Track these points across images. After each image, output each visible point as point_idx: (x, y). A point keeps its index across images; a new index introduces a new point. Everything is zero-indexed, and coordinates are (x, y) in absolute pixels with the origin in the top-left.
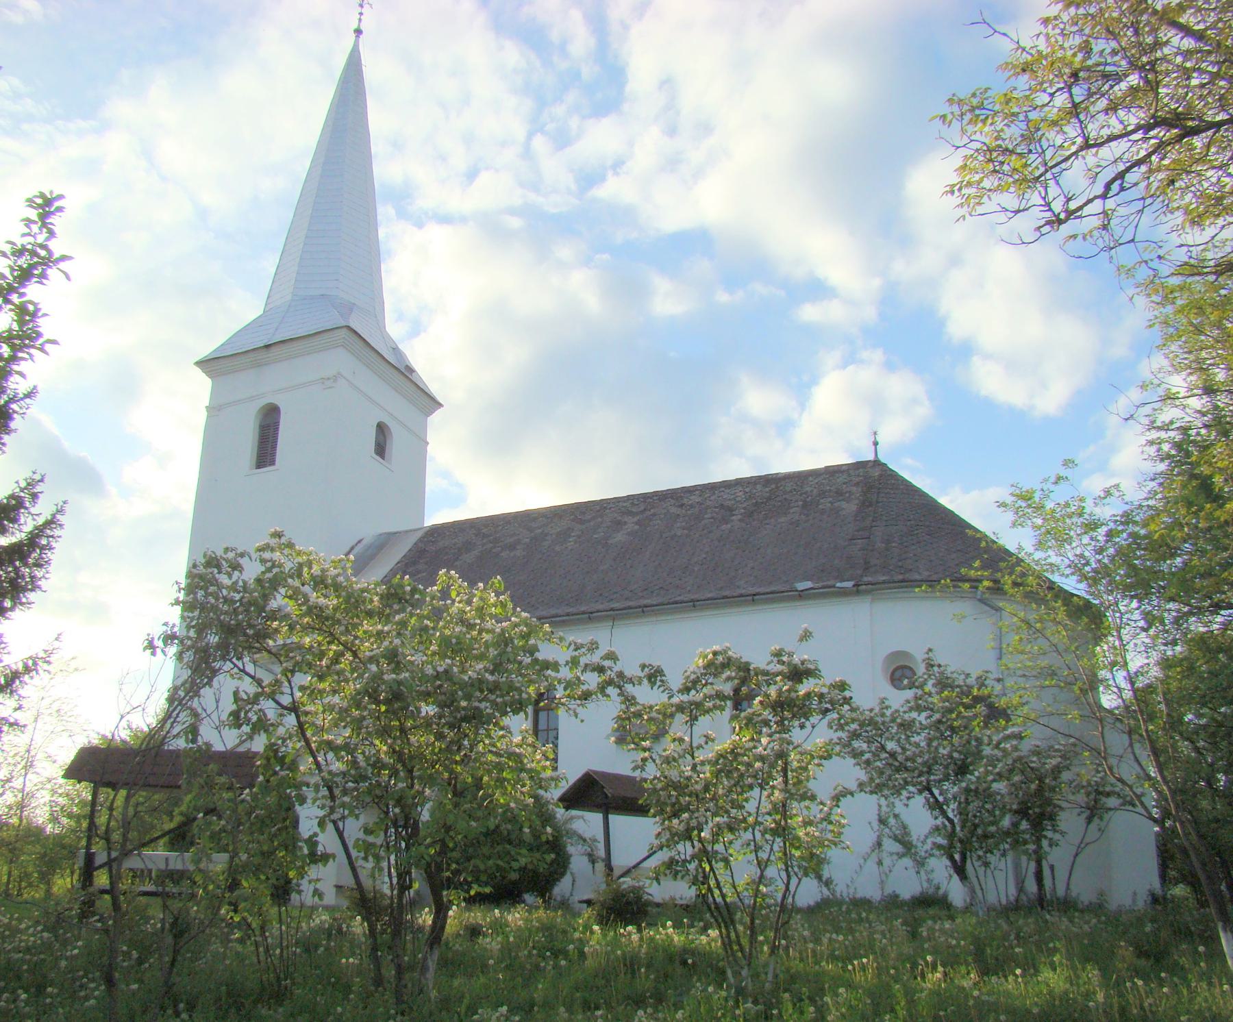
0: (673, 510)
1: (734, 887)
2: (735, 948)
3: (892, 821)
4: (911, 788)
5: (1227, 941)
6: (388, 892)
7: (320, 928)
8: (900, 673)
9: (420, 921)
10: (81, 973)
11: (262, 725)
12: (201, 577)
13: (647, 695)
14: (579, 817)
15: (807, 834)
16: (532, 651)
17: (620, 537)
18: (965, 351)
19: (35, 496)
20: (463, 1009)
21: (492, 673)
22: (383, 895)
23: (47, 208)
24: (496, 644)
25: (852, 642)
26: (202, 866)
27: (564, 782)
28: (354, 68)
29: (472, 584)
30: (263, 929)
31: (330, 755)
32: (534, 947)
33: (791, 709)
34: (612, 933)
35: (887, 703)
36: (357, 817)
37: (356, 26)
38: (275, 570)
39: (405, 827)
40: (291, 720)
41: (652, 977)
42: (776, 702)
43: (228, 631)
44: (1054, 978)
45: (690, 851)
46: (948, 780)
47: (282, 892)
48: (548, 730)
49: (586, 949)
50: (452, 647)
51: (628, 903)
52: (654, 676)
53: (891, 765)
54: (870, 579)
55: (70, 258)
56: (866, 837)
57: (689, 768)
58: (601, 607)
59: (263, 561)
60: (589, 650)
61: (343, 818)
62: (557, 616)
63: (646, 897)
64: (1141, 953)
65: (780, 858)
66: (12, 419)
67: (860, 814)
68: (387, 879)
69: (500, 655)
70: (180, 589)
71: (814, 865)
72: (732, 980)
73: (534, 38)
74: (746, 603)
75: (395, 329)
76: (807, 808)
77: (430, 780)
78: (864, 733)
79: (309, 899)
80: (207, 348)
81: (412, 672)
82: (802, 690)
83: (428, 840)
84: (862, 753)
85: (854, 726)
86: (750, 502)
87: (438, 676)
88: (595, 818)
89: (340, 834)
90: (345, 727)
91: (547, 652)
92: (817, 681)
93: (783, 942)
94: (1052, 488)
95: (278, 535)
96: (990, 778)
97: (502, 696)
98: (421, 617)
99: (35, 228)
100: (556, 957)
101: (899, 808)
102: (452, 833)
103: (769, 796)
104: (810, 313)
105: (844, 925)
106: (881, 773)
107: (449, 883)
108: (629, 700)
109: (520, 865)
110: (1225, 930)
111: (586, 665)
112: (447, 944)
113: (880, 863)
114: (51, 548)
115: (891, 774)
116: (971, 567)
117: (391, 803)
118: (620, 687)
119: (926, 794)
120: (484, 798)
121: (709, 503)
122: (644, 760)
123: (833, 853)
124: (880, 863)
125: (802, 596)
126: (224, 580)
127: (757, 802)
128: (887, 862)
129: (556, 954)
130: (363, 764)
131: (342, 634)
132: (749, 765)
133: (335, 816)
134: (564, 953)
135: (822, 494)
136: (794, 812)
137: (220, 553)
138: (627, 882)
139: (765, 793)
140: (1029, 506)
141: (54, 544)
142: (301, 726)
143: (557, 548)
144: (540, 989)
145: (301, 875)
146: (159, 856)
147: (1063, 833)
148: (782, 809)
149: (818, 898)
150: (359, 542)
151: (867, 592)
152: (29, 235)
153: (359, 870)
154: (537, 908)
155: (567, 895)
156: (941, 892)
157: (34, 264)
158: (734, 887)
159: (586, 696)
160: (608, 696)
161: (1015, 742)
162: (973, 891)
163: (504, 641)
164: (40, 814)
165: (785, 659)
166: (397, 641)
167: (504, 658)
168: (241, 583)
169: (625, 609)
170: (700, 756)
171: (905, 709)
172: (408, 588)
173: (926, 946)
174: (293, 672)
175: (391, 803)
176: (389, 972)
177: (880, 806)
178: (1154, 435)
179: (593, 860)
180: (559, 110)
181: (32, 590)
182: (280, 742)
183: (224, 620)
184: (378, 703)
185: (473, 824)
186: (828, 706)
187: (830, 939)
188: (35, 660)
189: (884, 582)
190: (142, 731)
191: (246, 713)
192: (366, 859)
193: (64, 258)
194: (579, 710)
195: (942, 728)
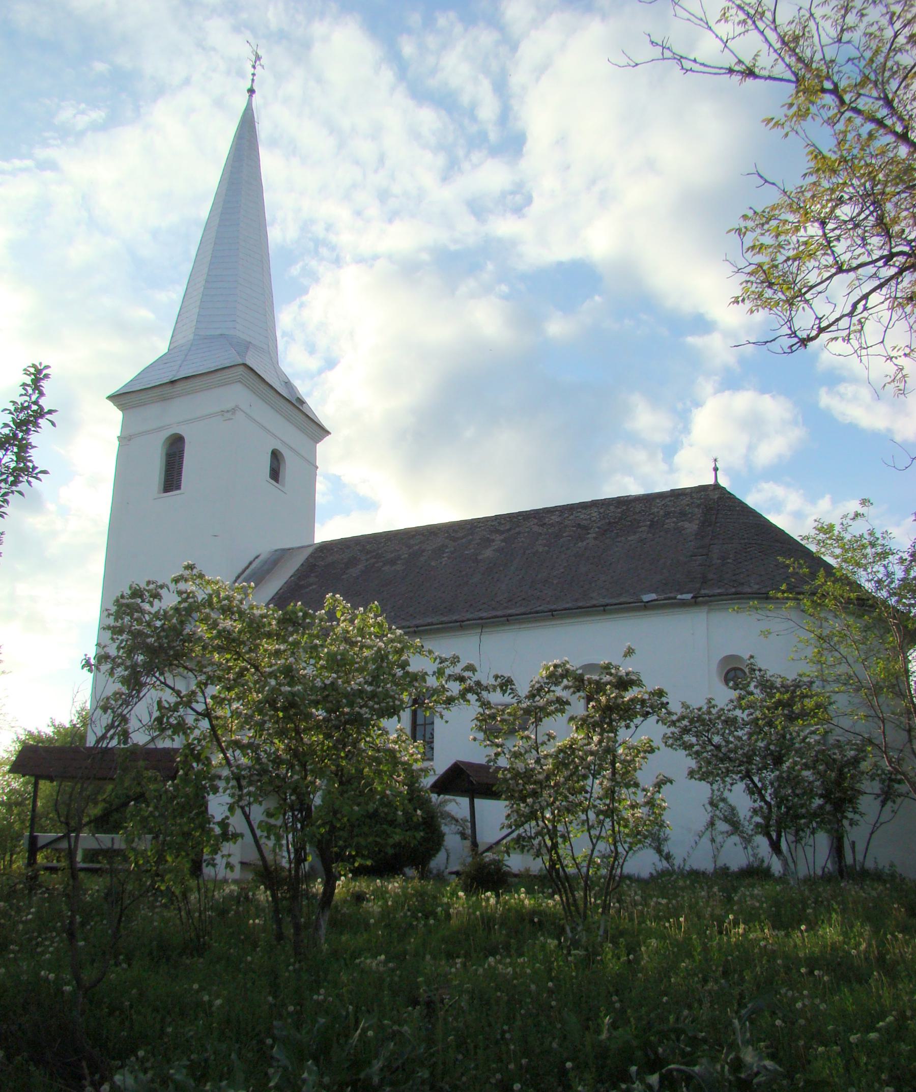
0: (536, 529)
1: (574, 859)
2: (573, 908)
3: (721, 805)
6: (287, 866)
8: (735, 673)
9: (314, 890)
10: (36, 934)
11: (181, 728)
12: (127, 606)
14: (450, 801)
16: (404, 665)
17: (488, 553)
21: (370, 684)
22: (282, 868)
23: (38, 377)
24: (374, 660)
25: (680, 654)
26: (134, 845)
27: (432, 773)
28: (247, 130)
29: (355, 607)
31: (238, 752)
32: (409, 910)
34: (474, 899)
35: (713, 702)
36: (260, 803)
37: (249, 87)
38: (190, 600)
39: (301, 811)
40: (205, 724)
41: (504, 932)
43: (152, 652)
44: (830, 933)
46: (766, 769)
47: (197, 868)
48: (425, 725)
49: (451, 911)
50: (337, 663)
52: (506, 684)
53: (716, 756)
54: (706, 592)
55: (55, 411)
57: (533, 761)
58: (470, 616)
59: (180, 593)
60: (452, 663)
61: (249, 804)
62: (432, 624)
63: (505, 868)
68: (285, 854)
69: (377, 669)
70: (109, 615)
72: (570, 935)
74: (598, 613)
76: (634, 793)
77: (320, 773)
81: (304, 684)
82: (628, 696)
83: (319, 822)
85: (685, 722)
86: (603, 522)
87: (325, 687)
88: (464, 801)
90: (249, 729)
92: (640, 689)
93: (617, 905)
94: (851, 522)
95: (190, 567)
98: (310, 636)
99: (30, 391)
102: (339, 816)
103: (601, 784)
106: (709, 763)
107: (340, 857)
108: (485, 704)
109: (400, 836)
111: (450, 676)
112: (336, 907)
113: (713, 840)
115: (715, 764)
116: (779, 590)
118: (477, 694)
121: (567, 522)
122: (497, 754)
125: (647, 607)
126: (146, 606)
128: (719, 839)
130: (264, 760)
131: (247, 653)
132: (582, 759)
134: (434, 914)
135: (667, 515)
136: (623, 797)
137: (143, 585)
138: (489, 856)
140: (830, 538)
142: (213, 728)
143: (433, 564)
144: (413, 942)
145: (215, 851)
147: (862, 814)
148: (610, 793)
150: (257, 557)
151: (704, 603)
152: (25, 395)
153: (263, 847)
155: (442, 868)
156: (765, 865)
157: (29, 418)
158: (574, 859)
159: (450, 701)
160: (469, 701)
163: (381, 657)
165: (613, 671)
166: (291, 660)
168: (162, 612)
169: (492, 618)
171: (730, 706)
172: (301, 614)
174: (206, 685)
176: (289, 931)
179: (463, 836)
182: (196, 742)
183: (146, 638)
184: (276, 710)
185: (356, 808)
186: (648, 709)
189: (720, 594)
190: (65, 728)
191: (168, 718)
192: (268, 837)
193: (50, 412)
194: (445, 712)
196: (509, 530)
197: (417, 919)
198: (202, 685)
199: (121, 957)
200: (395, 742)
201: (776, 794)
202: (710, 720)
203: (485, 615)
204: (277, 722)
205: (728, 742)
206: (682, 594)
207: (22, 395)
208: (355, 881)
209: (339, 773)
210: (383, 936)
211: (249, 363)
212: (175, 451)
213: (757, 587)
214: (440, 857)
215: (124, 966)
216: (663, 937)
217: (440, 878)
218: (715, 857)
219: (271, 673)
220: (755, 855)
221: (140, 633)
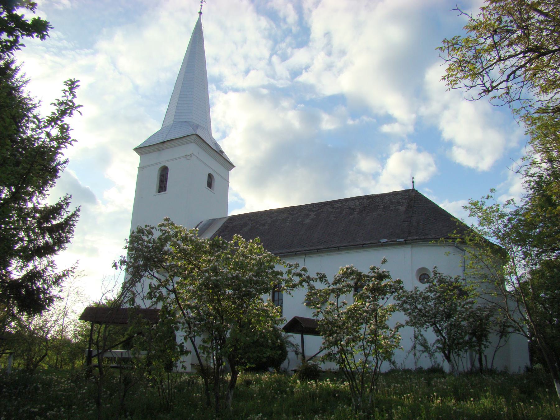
0: (330, 210)
3: (420, 337)
4: (428, 324)
6: (213, 367)
7: (185, 381)
8: (423, 276)
11: (161, 298)
14: (291, 336)
15: (385, 343)
16: (272, 267)
17: (308, 221)
18: (450, 144)
19: (67, 204)
20: (243, 415)
21: (255, 277)
22: (211, 368)
23: (72, 85)
24: (257, 265)
25: (403, 264)
29: (247, 240)
30: (161, 382)
31: (189, 310)
32: (273, 389)
33: (379, 291)
36: (200, 336)
38: (166, 234)
39: (220, 340)
40: (173, 296)
42: (372, 288)
43: (147, 259)
44: (486, 402)
45: (337, 350)
47: (169, 366)
49: (294, 390)
50: (239, 266)
52: (322, 278)
53: (419, 314)
56: (408, 344)
58: (300, 249)
61: (194, 336)
63: (319, 369)
67: (407, 335)
68: (212, 361)
70: (127, 242)
71: (388, 355)
72: (354, 403)
73: (273, 16)
76: (385, 332)
77: (230, 321)
78: (409, 301)
79: (180, 369)
80: (138, 144)
84: (408, 309)
85: (404, 298)
87: (233, 278)
89: (193, 343)
91: (278, 268)
95: (167, 220)
96: (460, 320)
97: (260, 286)
98: (226, 254)
99: (68, 94)
100: (282, 393)
101: (423, 332)
102: (239, 343)
103: (369, 327)
104: (386, 129)
105: (400, 380)
106: (415, 318)
107: (238, 363)
108: (312, 288)
109: (266, 352)
110: (557, 383)
111: (294, 273)
112: (237, 388)
113: (415, 355)
114: (74, 225)
115: (419, 319)
116: (452, 233)
121: (344, 207)
122: (318, 312)
123: (396, 351)
124: (415, 355)
125: (383, 245)
126: (146, 238)
127: (364, 329)
128: (418, 354)
129: (282, 392)
130: (202, 314)
131: (194, 260)
132: (361, 314)
134: (286, 392)
137: (143, 227)
138: (311, 362)
139: (368, 326)
140: (476, 208)
141: (75, 224)
142: (177, 298)
145: (177, 359)
147: (490, 342)
148: (374, 333)
149: (390, 369)
152: (65, 96)
154: (274, 373)
155: (286, 368)
156: (440, 366)
159: (294, 286)
161: (470, 305)
164: (70, 335)
165: (376, 271)
166: (216, 264)
168: (152, 240)
170: (341, 311)
174: (174, 276)
177: (415, 331)
178: (527, 179)
180: (283, 45)
181: (66, 243)
183: (145, 254)
184: (209, 289)
185: (248, 338)
186: (394, 290)
187: (394, 386)
188: (68, 271)
189: (417, 239)
190: (111, 300)
191: (154, 293)
192: (203, 353)
193: (79, 106)
194: (291, 292)
195: (440, 299)
196: (317, 210)
197: (277, 394)
198: (172, 277)
199: (128, 413)
200: (266, 306)
201: (448, 334)
204: (209, 295)
205: (425, 308)
206: (399, 239)
207: (63, 97)
208: (246, 374)
209: (239, 321)
211: (198, 134)
212: (164, 174)
213: (434, 236)
214: (286, 363)
215: (129, 417)
217: (285, 372)
218: (416, 363)
219: (206, 270)
220: (435, 362)
221: (141, 250)
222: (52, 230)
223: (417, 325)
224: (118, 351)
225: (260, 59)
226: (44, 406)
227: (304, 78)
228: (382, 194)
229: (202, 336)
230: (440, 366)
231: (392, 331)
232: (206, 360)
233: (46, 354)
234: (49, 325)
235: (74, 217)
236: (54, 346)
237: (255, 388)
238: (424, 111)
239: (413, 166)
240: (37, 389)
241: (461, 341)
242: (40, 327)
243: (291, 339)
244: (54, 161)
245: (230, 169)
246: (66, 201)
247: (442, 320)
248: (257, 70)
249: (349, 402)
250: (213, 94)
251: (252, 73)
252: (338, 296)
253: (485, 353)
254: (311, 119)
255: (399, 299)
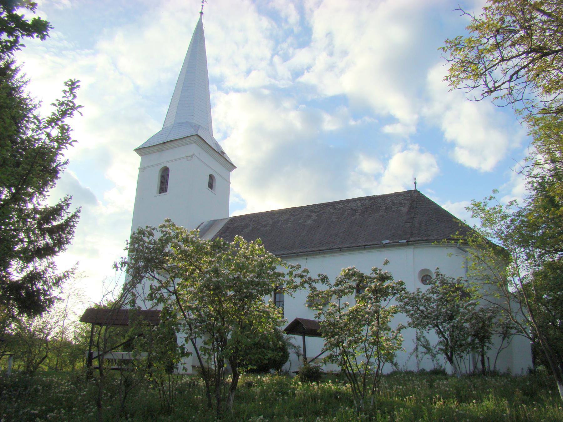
0: (332, 211)
2: (357, 391)
3: (422, 339)
4: (430, 326)
5: (561, 388)
6: (214, 368)
7: (186, 383)
8: (425, 278)
9: (227, 380)
11: (162, 299)
13: (321, 287)
14: (293, 337)
15: (387, 344)
16: (273, 269)
17: (310, 222)
18: (452, 145)
19: (68, 205)
21: (257, 278)
22: (212, 370)
23: (73, 85)
24: (259, 266)
25: (406, 265)
29: (249, 241)
30: (162, 384)
31: (190, 312)
33: (380, 293)
36: (201, 337)
37: (200, 11)
38: (167, 236)
39: (221, 341)
40: (174, 297)
43: (148, 261)
45: (338, 351)
47: (170, 368)
48: (280, 301)
49: (296, 392)
50: (240, 267)
51: (313, 373)
52: (324, 279)
53: (422, 316)
56: (411, 346)
58: (302, 251)
61: (195, 338)
63: (320, 370)
64: (525, 394)
65: (376, 355)
66: (58, 173)
67: (409, 336)
68: (213, 363)
69: (260, 270)
70: (128, 243)
71: (390, 357)
72: (356, 405)
73: (275, 16)
74: (362, 249)
75: (217, 136)
76: (387, 333)
77: (231, 322)
78: (411, 303)
79: (181, 371)
80: (139, 144)
83: (230, 347)
84: (410, 311)
85: (406, 300)
89: (194, 344)
91: (280, 269)
95: (168, 221)
96: (463, 321)
97: (261, 287)
98: (227, 255)
99: (68, 94)
100: (283, 395)
101: (425, 334)
102: (240, 344)
104: (388, 129)
105: (402, 382)
106: (418, 319)
107: (239, 365)
108: (314, 289)
109: (268, 356)
110: (560, 384)
111: (296, 275)
113: (417, 356)
114: (75, 226)
115: (421, 320)
116: (455, 234)
117: (215, 332)
118: (310, 284)
119: (436, 328)
120: (253, 330)
121: (346, 208)
122: (320, 314)
123: (398, 352)
124: (417, 356)
125: (385, 246)
126: (146, 239)
127: (366, 331)
128: (420, 356)
129: (284, 393)
130: (203, 315)
131: (195, 262)
132: (363, 316)
133: (192, 337)
134: (287, 393)
137: (144, 228)
138: (313, 364)
139: (370, 327)
140: (479, 209)
141: (76, 225)
142: (178, 300)
145: (178, 361)
146: (119, 353)
147: (493, 344)
148: (376, 334)
149: (392, 371)
152: (65, 97)
155: (288, 369)
156: (442, 368)
159: (296, 287)
161: (473, 307)
162: (455, 368)
163: (261, 264)
164: (70, 336)
165: (378, 272)
166: (218, 265)
167: (262, 272)
168: (153, 241)
170: (343, 312)
172: (222, 243)
173: (436, 390)
174: (174, 277)
175: (215, 332)
176: (214, 402)
178: (530, 180)
180: (285, 46)
181: (67, 244)
183: (146, 256)
184: (210, 290)
185: (249, 340)
186: (396, 291)
187: (397, 388)
188: (68, 272)
189: (419, 240)
190: (112, 302)
191: (155, 294)
192: (205, 355)
193: (80, 107)
194: (293, 293)
196: (319, 212)
198: (173, 278)
201: (451, 335)
202: (419, 299)
203: (308, 250)
204: (210, 297)
207: (63, 97)
208: (247, 376)
209: (241, 323)
210: (262, 405)
211: (199, 134)
212: (165, 175)
213: (436, 237)
214: (288, 363)
216: (405, 407)
218: (418, 364)
219: (207, 272)
222: (52, 231)
223: (420, 327)
224: (119, 353)
225: (262, 59)
226: (44, 408)
227: (306, 78)
228: (384, 195)
229: (203, 337)
230: (442, 368)
231: (394, 332)
232: (207, 362)
233: (46, 356)
234: (49, 326)
235: (75, 218)
236: (55, 348)
237: (256, 389)
238: (426, 111)
239: (415, 167)
240: (37, 391)
241: (464, 342)
242: (40, 329)
243: (292, 341)
244: (54, 161)
245: (231, 170)
246: (67, 202)
247: (445, 321)
248: (259, 70)
249: (351, 403)
250: (214, 94)
251: (254, 74)
252: (340, 297)
253: (488, 355)
254: (313, 119)
255: (401, 300)
